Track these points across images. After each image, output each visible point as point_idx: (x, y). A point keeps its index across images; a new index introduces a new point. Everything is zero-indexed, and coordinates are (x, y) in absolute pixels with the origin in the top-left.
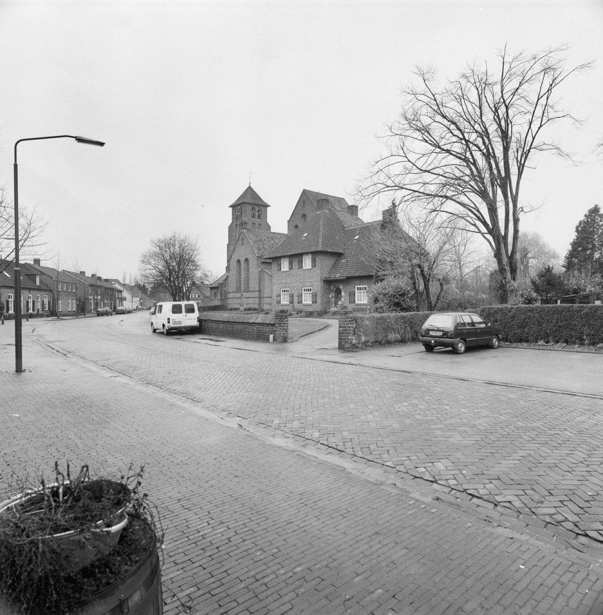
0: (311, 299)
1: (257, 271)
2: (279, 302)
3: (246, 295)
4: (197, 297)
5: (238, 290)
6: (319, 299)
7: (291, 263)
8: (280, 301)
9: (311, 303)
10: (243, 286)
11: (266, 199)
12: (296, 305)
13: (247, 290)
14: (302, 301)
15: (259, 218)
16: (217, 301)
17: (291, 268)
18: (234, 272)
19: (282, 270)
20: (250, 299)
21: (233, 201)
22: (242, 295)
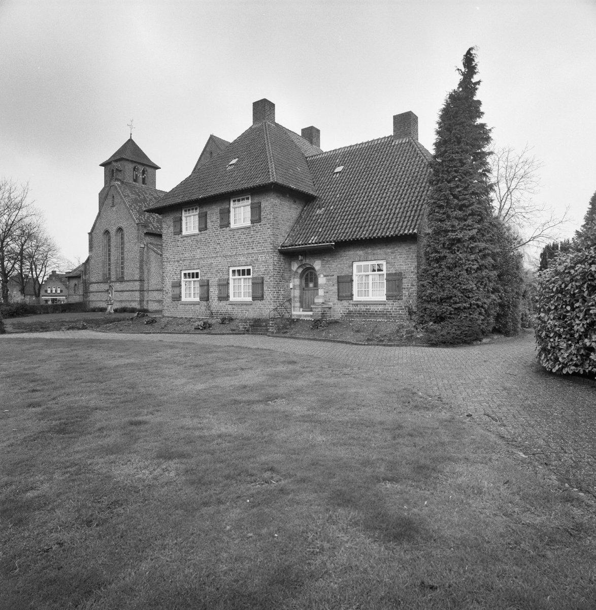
0: (198, 291)
1: (136, 248)
2: (177, 298)
3: (118, 286)
4: (59, 292)
5: (107, 280)
6: (269, 294)
7: (203, 218)
8: (180, 297)
9: (250, 299)
10: (113, 273)
11: (154, 159)
12: (215, 303)
13: (121, 280)
14: (228, 296)
15: (144, 182)
16: (78, 297)
17: (203, 228)
18: (100, 250)
19: (184, 233)
20: (125, 293)
21: (106, 157)
22: (110, 286)
